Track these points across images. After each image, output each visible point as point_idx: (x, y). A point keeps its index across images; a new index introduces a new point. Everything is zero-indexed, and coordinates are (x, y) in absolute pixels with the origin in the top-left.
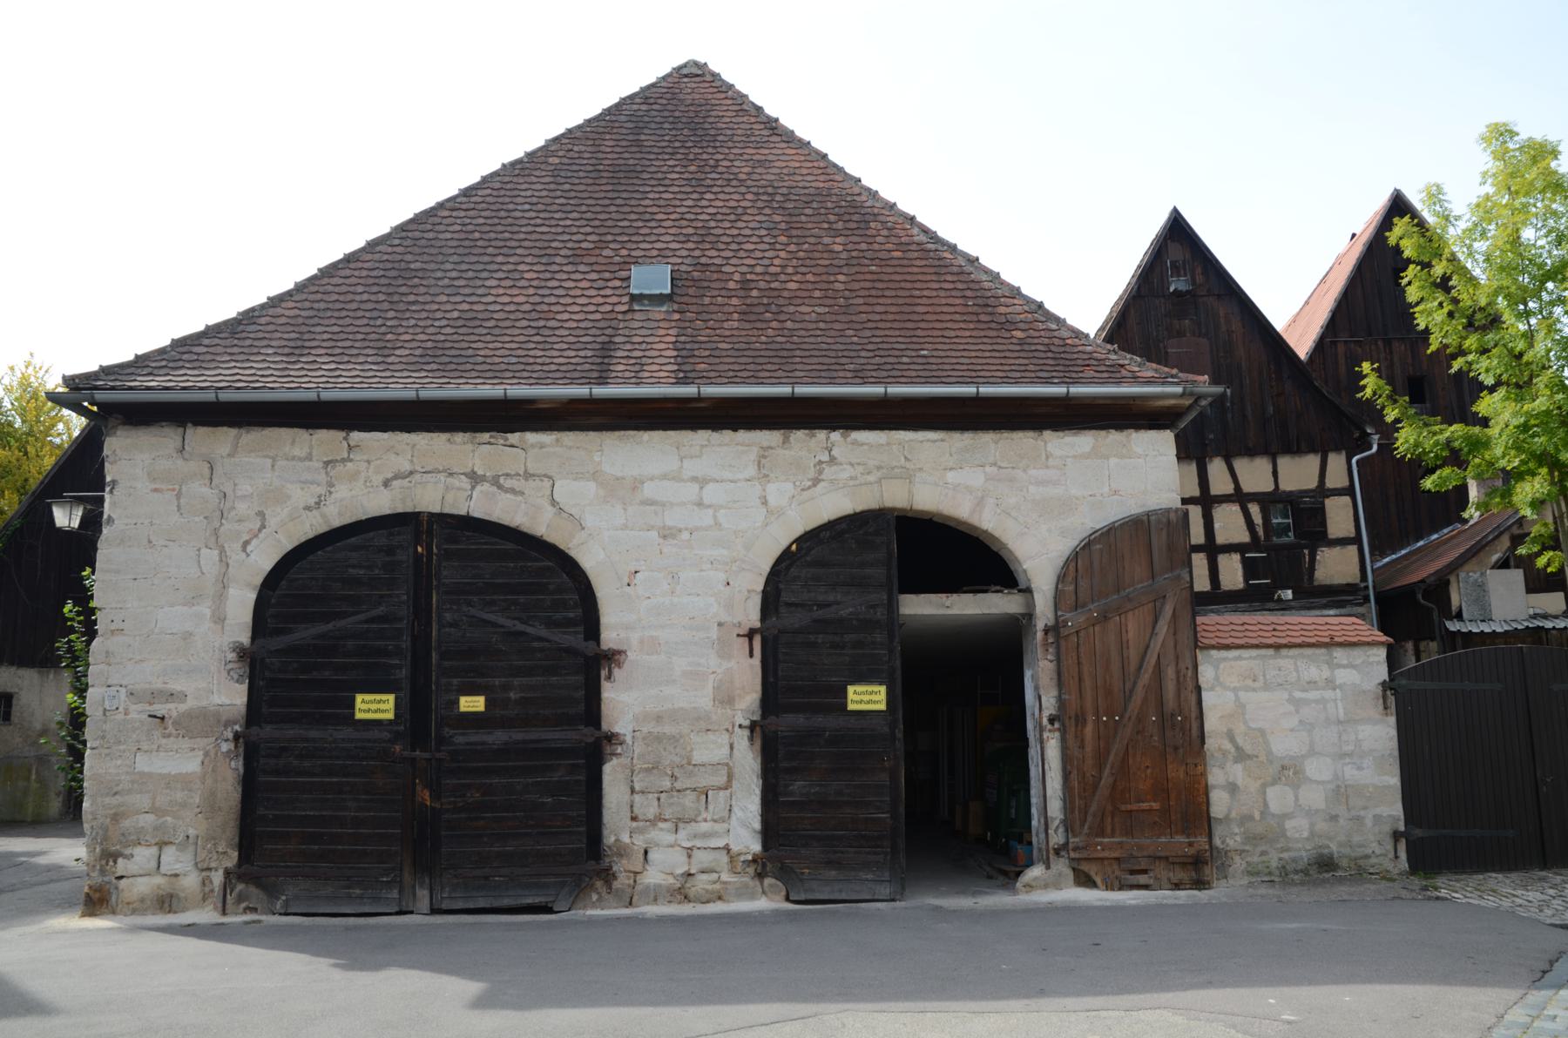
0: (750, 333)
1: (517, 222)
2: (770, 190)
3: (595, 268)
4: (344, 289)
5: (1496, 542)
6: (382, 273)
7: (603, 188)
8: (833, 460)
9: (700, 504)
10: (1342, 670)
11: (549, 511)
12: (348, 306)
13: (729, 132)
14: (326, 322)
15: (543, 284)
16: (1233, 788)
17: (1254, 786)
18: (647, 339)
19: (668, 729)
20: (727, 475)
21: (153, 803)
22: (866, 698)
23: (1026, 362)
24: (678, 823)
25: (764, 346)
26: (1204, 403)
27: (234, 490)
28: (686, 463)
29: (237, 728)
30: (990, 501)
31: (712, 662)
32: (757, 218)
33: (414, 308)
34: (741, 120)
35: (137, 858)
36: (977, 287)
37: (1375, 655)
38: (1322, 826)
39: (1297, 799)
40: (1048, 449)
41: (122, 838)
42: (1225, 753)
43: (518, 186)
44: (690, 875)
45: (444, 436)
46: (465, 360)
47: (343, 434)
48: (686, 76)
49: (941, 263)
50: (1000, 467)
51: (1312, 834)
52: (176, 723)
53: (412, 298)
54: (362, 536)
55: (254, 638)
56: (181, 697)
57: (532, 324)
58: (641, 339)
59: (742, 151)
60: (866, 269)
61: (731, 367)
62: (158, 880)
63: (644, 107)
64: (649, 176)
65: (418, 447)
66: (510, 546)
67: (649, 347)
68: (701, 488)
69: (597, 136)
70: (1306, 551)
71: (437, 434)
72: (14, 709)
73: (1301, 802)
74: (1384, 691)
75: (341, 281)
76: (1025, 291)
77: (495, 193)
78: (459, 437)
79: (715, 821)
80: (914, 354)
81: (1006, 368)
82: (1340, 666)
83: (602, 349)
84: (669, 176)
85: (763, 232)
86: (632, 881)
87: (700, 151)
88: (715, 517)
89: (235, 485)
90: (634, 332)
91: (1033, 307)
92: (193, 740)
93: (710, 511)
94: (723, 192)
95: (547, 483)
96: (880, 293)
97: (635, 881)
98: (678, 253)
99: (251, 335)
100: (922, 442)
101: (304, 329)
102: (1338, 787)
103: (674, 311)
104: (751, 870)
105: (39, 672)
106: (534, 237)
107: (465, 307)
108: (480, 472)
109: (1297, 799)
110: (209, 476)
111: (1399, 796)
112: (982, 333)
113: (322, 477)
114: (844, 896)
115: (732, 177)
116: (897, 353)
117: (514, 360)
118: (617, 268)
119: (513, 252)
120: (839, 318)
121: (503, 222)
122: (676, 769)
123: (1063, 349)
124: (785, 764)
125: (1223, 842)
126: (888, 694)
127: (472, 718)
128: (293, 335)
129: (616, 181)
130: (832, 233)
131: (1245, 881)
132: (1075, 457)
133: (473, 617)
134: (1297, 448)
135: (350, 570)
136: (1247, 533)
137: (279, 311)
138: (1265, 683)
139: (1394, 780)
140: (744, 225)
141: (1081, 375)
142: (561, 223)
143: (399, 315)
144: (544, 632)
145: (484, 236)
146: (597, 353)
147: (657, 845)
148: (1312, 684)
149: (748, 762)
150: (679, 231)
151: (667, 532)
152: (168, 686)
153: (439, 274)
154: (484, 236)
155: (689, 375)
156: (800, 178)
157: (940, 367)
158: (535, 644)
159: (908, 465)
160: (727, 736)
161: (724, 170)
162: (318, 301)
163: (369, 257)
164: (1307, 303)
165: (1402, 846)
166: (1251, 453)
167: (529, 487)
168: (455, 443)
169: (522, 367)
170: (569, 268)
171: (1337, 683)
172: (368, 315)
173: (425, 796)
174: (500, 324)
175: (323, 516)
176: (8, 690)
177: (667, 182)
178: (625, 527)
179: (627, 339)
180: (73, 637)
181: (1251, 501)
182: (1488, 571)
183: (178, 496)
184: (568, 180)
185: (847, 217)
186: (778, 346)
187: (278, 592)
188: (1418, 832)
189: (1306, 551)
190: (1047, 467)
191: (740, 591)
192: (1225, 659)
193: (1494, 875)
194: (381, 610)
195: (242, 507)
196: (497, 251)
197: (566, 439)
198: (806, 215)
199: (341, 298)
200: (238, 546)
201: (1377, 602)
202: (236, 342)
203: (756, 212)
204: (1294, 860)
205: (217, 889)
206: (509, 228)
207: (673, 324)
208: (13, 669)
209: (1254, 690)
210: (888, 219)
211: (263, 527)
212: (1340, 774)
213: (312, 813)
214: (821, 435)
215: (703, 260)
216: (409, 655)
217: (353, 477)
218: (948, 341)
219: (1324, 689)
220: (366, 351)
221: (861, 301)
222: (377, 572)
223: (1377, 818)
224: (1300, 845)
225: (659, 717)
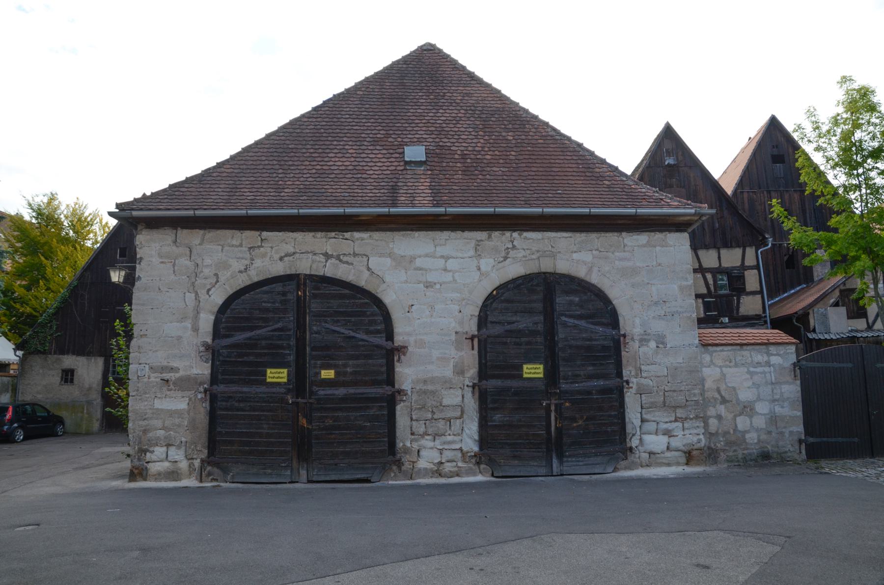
0: (468, 181)
1: (343, 124)
2: (473, 108)
3: (385, 147)
4: (256, 158)
5: (832, 293)
6: (274, 150)
7: (386, 107)
8: (514, 247)
9: (445, 270)
11: (366, 274)
12: (258, 167)
13: (449, 79)
14: (247, 175)
15: (359, 156)
16: (719, 417)
17: (730, 416)
18: (415, 184)
19: (430, 387)
20: (461, 255)
21: (164, 425)
23: (612, 197)
24: (435, 436)
25: (476, 188)
26: (704, 218)
27: (202, 262)
28: (438, 249)
29: (206, 386)
30: (595, 269)
31: (453, 352)
32: (467, 122)
33: (292, 168)
34: (455, 72)
35: (155, 453)
36: (583, 158)
37: (789, 349)
38: (764, 437)
39: (751, 423)
41: (148, 442)
42: (715, 399)
43: (342, 106)
44: (442, 463)
45: (311, 234)
46: (321, 194)
47: (258, 233)
48: (425, 50)
49: (564, 146)
51: (759, 441)
52: (174, 383)
53: (291, 163)
54: (270, 286)
55: (213, 339)
56: (176, 370)
57: (354, 176)
58: (412, 184)
59: (457, 88)
60: (526, 149)
61: (461, 198)
62: (166, 464)
63: (404, 66)
64: (410, 101)
65: (297, 240)
66: (347, 291)
67: (416, 188)
68: (446, 261)
69: (382, 81)
70: (735, 298)
71: (307, 233)
72: (75, 377)
74: (795, 367)
75: (253, 154)
76: (608, 161)
77: (331, 109)
78: (319, 234)
79: (454, 435)
80: (554, 192)
81: (603, 200)
82: (772, 355)
83: (392, 189)
84: (420, 101)
85: (471, 130)
86: (412, 466)
87: (436, 88)
88: (453, 277)
89: (203, 260)
90: (408, 180)
91: (613, 169)
92: (183, 393)
93: (451, 274)
94: (449, 109)
95: (365, 259)
96: (534, 161)
97: (413, 466)
98: (428, 140)
99: (209, 182)
100: (560, 238)
101: (236, 179)
102: (772, 417)
103: (428, 170)
104: (473, 461)
105: (87, 359)
106: (352, 131)
107: (319, 167)
108: (330, 253)
109: (751, 423)
110: (189, 255)
111: (802, 422)
112: (588, 182)
113: (248, 256)
114: (522, 474)
115: (453, 101)
116: (546, 192)
117: (347, 194)
118: (396, 147)
119: (341, 139)
120: (514, 174)
121: (336, 124)
123: (630, 191)
124: (491, 406)
125: (715, 445)
126: (544, 369)
128: (231, 182)
129: (393, 103)
130: (507, 130)
131: (725, 465)
132: (638, 246)
133: (328, 328)
134: (727, 245)
135: (263, 304)
136: (705, 289)
137: (223, 170)
138: (735, 364)
139: (800, 414)
140: (461, 126)
141: (641, 204)
142: (366, 124)
143: (284, 171)
144: (365, 337)
145: (326, 131)
146: (390, 191)
147: (425, 448)
149: (471, 404)
150: (427, 129)
151: (428, 285)
152: (170, 364)
153: (304, 151)
154: (326, 131)
155: (439, 202)
156: (488, 102)
157: (569, 199)
158: (360, 343)
161: (449, 98)
162: (242, 165)
163: (268, 142)
164: (725, 172)
165: (803, 446)
166: (707, 247)
167: (355, 260)
168: (317, 237)
169: (351, 198)
170: (371, 148)
171: (771, 363)
172: (268, 171)
173: (303, 422)
174: (338, 176)
175: (248, 276)
176: (72, 367)
177: (419, 104)
178: (406, 282)
179: (404, 184)
180: (118, 338)
181: (708, 272)
182: (828, 308)
183: (174, 265)
184: (368, 103)
185: (513, 122)
186: (484, 188)
187: (226, 315)
188: (811, 440)
189: (735, 298)
190: (624, 251)
191: (466, 316)
192: (716, 351)
193: (848, 461)
194: (279, 325)
195: (206, 271)
196: (334, 139)
197: (375, 235)
198: (493, 121)
199: (254, 163)
200: (204, 291)
201: (771, 324)
202: (202, 185)
203: (466, 119)
204: (750, 454)
205: (197, 469)
206: (339, 127)
207: (428, 176)
208: (74, 357)
209: (730, 367)
210: (535, 123)
211: (217, 281)
212: (773, 411)
213: (245, 431)
214: (508, 234)
215: (441, 144)
216: (295, 349)
217: (264, 255)
218: (571, 186)
219: (764, 366)
220: (269, 190)
221: (524, 165)
222: (277, 305)
223: (791, 433)
224: (753, 447)
225: (425, 381)
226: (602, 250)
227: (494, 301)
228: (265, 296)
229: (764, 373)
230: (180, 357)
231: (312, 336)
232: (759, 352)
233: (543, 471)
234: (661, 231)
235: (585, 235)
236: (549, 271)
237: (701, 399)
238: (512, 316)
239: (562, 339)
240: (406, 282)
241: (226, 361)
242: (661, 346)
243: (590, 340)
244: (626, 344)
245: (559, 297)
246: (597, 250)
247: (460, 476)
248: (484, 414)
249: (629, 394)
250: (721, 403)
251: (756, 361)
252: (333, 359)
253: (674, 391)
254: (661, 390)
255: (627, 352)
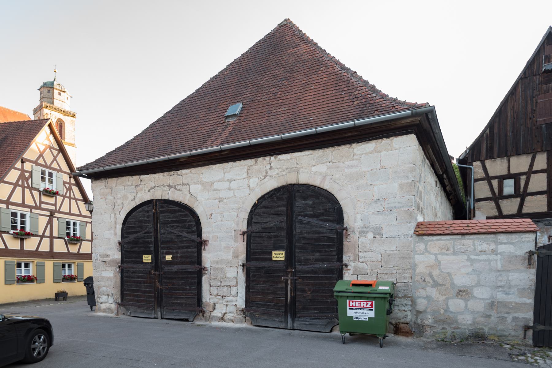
9: (230, 189)
10: (503, 245)
19: (220, 266)
20: (238, 178)
22: (278, 256)
28: (226, 175)
30: (328, 177)
31: (232, 243)
39: (466, 306)
40: (354, 152)
45: (162, 174)
50: (334, 163)
51: (474, 323)
66: (177, 208)
73: (469, 307)
82: (501, 243)
88: (234, 193)
93: (232, 191)
100: (303, 156)
108: (171, 185)
109: (466, 306)
113: (135, 191)
122: (222, 279)
124: (252, 279)
125: (422, 322)
127: (169, 263)
132: (366, 153)
133: (168, 231)
135: (140, 218)
138: (454, 251)
148: (483, 252)
149: (242, 277)
159: (298, 166)
160: (236, 269)
165: (530, 333)
171: (499, 252)
173: (158, 284)
175: (135, 202)
178: (208, 199)
187: (126, 226)
188: (541, 327)
190: (353, 160)
191: (241, 219)
195: (119, 201)
209: (447, 254)
214: (268, 158)
217: (141, 190)
219: (490, 254)
222: (145, 218)
223: (515, 319)
226: (334, 161)
227: (257, 207)
228: (140, 213)
229: (489, 261)
230: (110, 249)
231: (161, 235)
232: (485, 241)
233: (282, 326)
234: (388, 137)
235: (322, 150)
236: (293, 183)
237: (410, 281)
238: (266, 218)
239: (298, 233)
240: (208, 199)
241: (127, 251)
242: (377, 236)
243: (319, 233)
244: (347, 235)
245: (298, 202)
246: (331, 162)
247: (234, 323)
248: (248, 284)
249: (347, 274)
250: (432, 287)
251: (480, 249)
252: (171, 249)
253: (386, 274)
254: (374, 273)
255: (349, 242)
